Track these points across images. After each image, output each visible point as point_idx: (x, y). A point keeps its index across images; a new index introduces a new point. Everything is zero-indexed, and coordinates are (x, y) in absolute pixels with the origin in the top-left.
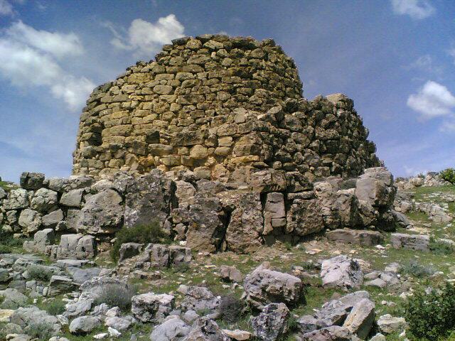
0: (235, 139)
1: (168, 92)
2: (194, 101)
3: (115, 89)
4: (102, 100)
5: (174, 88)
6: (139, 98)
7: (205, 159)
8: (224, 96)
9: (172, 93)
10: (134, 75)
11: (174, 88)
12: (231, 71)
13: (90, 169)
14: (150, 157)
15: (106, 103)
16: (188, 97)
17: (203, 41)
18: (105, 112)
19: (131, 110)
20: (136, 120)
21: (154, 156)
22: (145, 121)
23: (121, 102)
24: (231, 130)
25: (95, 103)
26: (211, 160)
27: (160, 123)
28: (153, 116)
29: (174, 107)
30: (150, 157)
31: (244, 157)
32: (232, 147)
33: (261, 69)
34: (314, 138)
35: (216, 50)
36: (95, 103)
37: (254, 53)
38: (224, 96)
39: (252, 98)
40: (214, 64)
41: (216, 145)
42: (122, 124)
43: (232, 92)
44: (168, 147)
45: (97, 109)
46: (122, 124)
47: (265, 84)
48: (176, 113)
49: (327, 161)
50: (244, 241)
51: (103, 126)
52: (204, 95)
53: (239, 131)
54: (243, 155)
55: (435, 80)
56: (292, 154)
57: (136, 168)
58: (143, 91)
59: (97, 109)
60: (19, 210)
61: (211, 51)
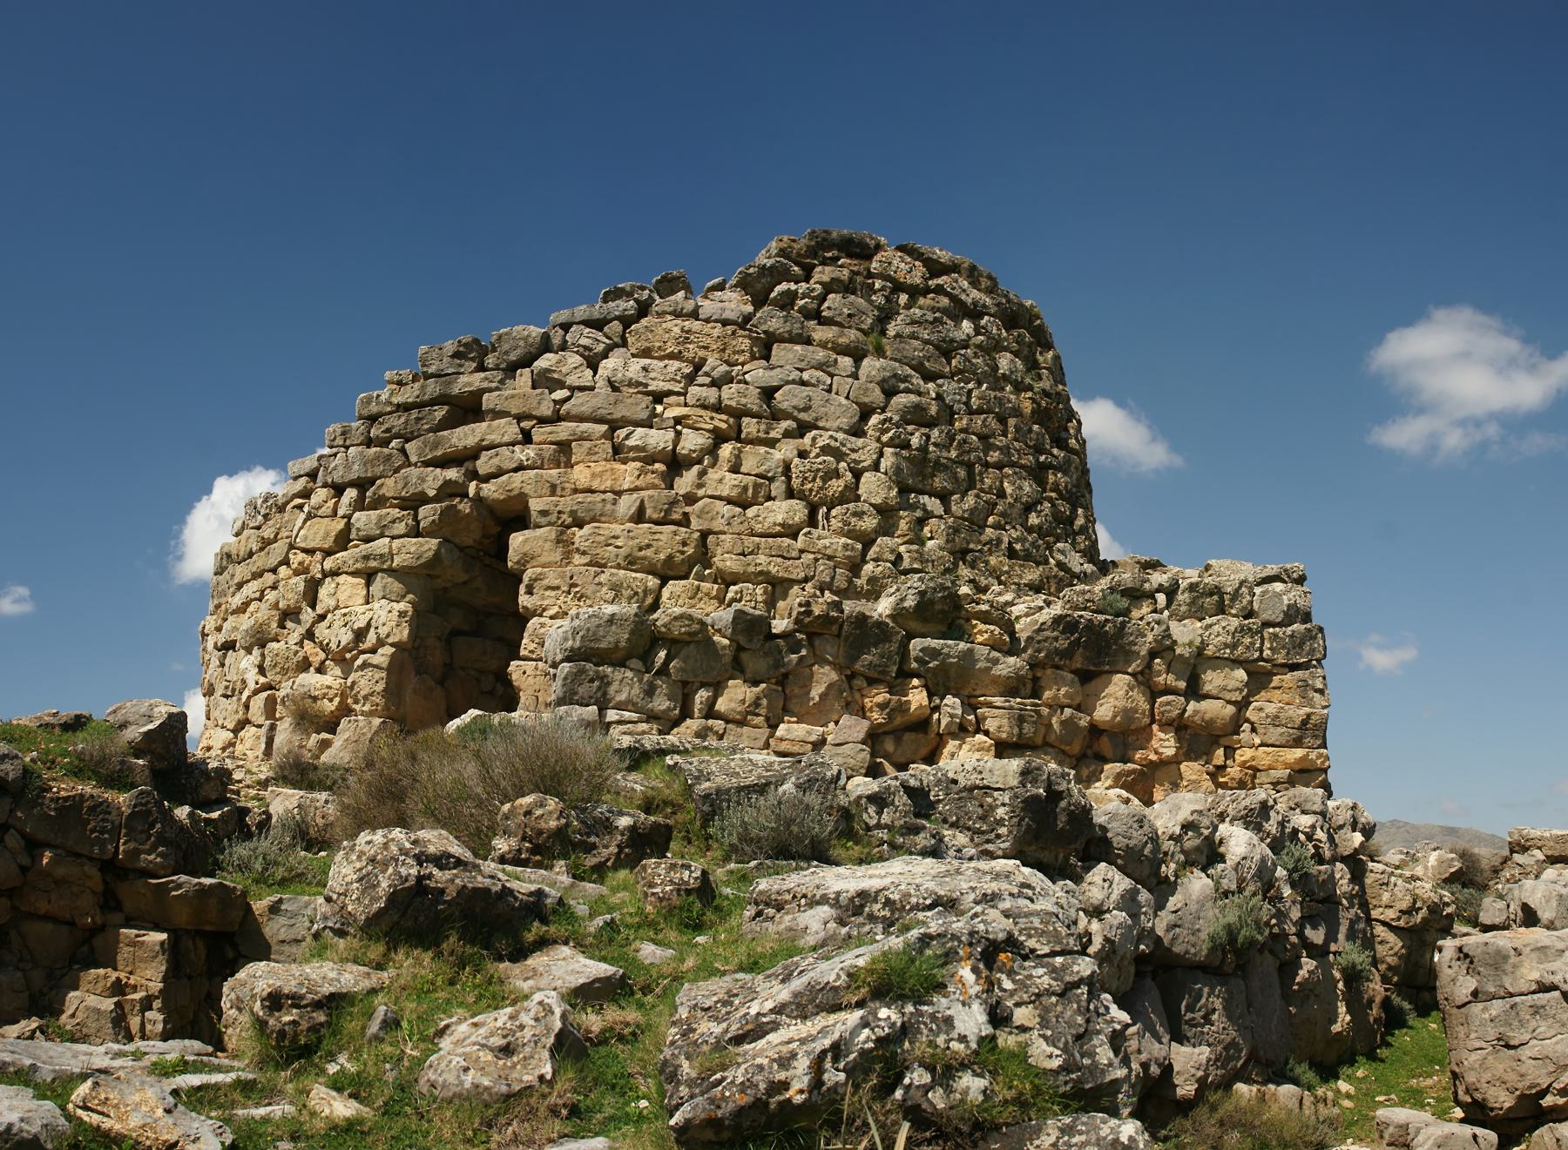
0: (1259, 679)
1: (844, 422)
2: (939, 482)
4: (488, 401)
5: (866, 412)
6: (721, 422)
7: (1142, 736)
11: (866, 412)
13: (612, 715)
15: (519, 418)
17: (935, 268)
18: (507, 458)
19: (675, 464)
21: (935, 691)
23: (614, 426)
24: (1247, 640)
25: (440, 413)
26: (1165, 744)
28: (792, 511)
31: (1299, 753)
32: (1242, 705)
36: (440, 413)
41: (1194, 691)
42: (639, 517)
44: (1010, 665)
46: (639, 517)
48: (886, 513)
52: (969, 466)
53: (1267, 653)
54: (1297, 743)
57: (861, 736)
58: (729, 394)
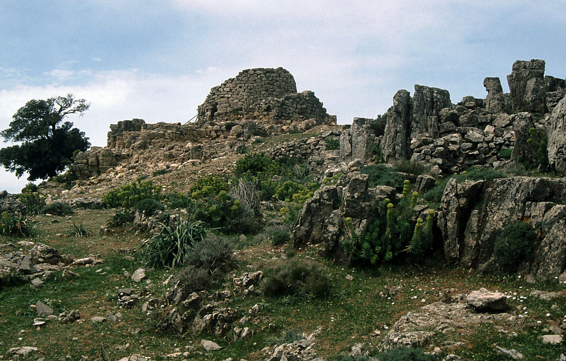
3: (221, 89)
8: (264, 92)
9: (244, 91)
10: (229, 84)
12: (266, 82)
14: (239, 116)
16: (251, 93)
19: (228, 98)
20: (230, 102)
22: (237, 103)
27: (240, 103)
29: (245, 97)
30: (239, 116)
33: (277, 81)
34: (297, 108)
35: (260, 74)
37: (274, 75)
38: (264, 92)
39: (274, 93)
40: (260, 80)
43: (267, 90)
45: (214, 97)
47: (279, 87)
49: (302, 116)
50: (523, 191)
51: (217, 104)
55: (558, 345)
56: (288, 114)
59: (214, 97)
60: (210, 131)
61: (258, 75)
